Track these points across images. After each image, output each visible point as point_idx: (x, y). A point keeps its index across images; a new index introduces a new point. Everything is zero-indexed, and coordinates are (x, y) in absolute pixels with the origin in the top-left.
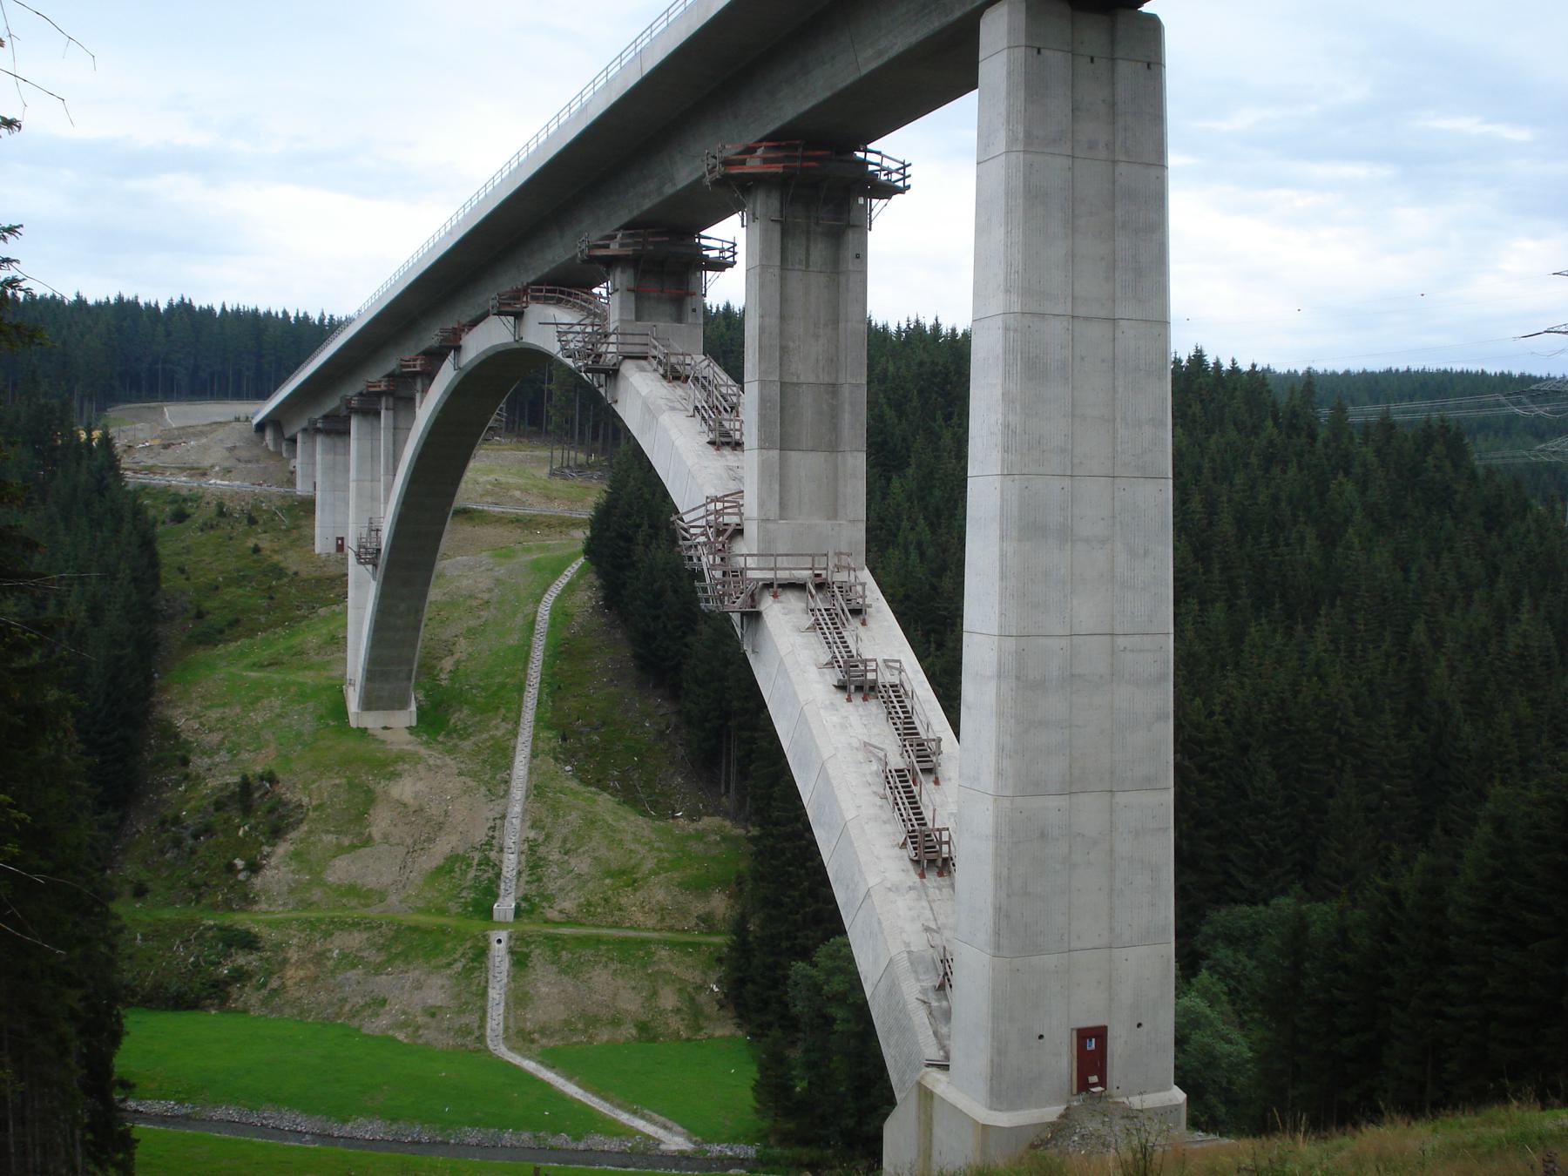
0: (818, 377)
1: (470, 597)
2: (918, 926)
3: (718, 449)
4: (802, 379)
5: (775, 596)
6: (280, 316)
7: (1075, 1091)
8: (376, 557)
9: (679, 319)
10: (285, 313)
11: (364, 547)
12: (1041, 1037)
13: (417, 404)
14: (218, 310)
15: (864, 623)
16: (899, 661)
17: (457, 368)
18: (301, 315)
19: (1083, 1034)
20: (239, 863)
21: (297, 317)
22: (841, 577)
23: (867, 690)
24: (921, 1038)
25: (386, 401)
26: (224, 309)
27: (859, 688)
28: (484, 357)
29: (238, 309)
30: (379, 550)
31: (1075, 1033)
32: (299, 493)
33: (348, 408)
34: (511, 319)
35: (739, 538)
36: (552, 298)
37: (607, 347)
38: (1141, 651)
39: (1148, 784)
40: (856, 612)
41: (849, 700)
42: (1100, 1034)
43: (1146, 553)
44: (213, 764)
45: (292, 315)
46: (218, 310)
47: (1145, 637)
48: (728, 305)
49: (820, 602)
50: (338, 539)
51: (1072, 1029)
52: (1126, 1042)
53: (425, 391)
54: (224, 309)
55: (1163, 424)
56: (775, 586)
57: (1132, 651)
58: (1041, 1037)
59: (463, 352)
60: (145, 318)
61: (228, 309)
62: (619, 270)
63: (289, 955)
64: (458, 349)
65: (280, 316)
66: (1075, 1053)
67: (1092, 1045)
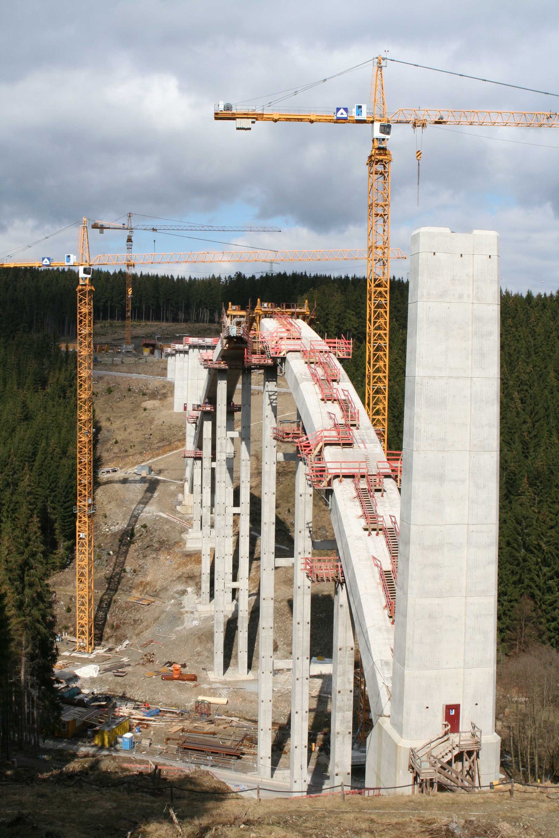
1: (83, 648)
6: (170, 277)
10: (172, 276)
12: (427, 708)
14: (139, 275)
16: (335, 415)
19: (449, 708)
26: (190, 278)
29: (148, 275)
32: (168, 380)
37: (424, 761)
42: (457, 707)
44: (17, 551)
45: (175, 278)
46: (139, 275)
48: (213, 275)
54: (141, 274)
56: (341, 476)
58: (427, 708)
61: (143, 274)
65: (170, 277)
67: (453, 713)
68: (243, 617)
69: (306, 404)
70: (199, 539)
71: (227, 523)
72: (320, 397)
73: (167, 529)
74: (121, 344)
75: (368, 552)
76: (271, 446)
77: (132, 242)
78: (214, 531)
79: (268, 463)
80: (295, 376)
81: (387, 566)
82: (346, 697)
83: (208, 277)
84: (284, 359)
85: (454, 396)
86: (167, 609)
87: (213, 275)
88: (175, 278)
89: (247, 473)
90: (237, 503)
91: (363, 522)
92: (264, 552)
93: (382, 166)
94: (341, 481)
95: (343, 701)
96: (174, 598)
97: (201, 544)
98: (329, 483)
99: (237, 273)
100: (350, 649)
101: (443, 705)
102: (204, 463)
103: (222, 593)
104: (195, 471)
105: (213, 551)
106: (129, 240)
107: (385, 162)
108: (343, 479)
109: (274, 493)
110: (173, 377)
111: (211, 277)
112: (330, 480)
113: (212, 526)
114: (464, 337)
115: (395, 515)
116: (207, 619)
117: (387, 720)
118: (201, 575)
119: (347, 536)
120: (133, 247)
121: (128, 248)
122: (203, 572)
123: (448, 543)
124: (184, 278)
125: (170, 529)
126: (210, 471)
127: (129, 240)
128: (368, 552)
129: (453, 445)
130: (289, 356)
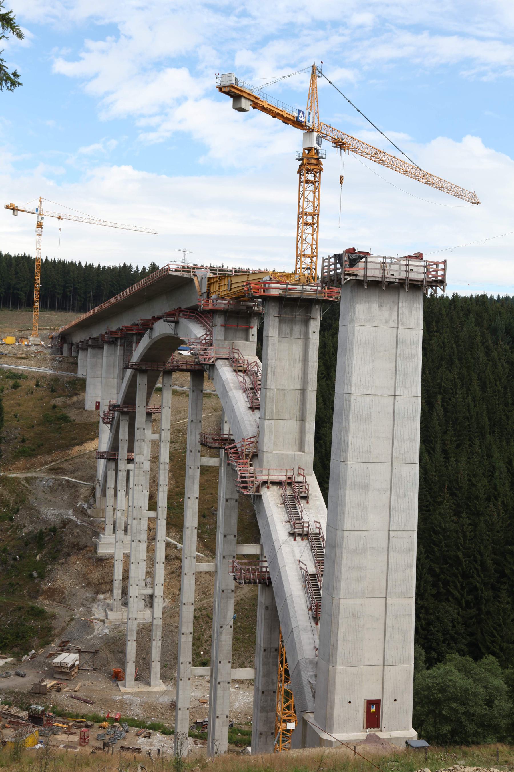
0: (294, 386)
2: (312, 647)
3: (253, 411)
4: (287, 388)
5: (268, 488)
6: (77, 265)
7: (365, 727)
8: (112, 421)
9: (247, 340)
10: (80, 263)
11: (106, 416)
12: (350, 702)
13: (134, 349)
15: (308, 502)
17: (150, 338)
18: (88, 264)
19: (370, 703)
20: (35, 574)
21: (86, 266)
22: (300, 479)
23: (305, 536)
24: (307, 698)
25: (121, 341)
27: (300, 535)
28: (162, 336)
29: (54, 261)
30: (114, 418)
31: (366, 701)
32: (79, 376)
33: (102, 341)
34: (173, 324)
35: (256, 458)
36: (193, 316)
38: (401, 538)
39: (404, 595)
40: (305, 498)
41: (295, 540)
42: (377, 703)
43: (405, 496)
45: (83, 265)
47: (403, 532)
48: (124, 264)
49: (289, 491)
50: (96, 402)
51: (364, 700)
52: (389, 707)
53: (138, 342)
55: (414, 440)
57: (397, 538)
58: (350, 702)
59: (154, 331)
60: (4, 264)
62: (217, 316)
63: (448, 657)
64: (152, 329)
65: (77, 265)
66: (366, 710)
68: (157, 625)
69: (235, 411)
70: (111, 543)
71: (142, 528)
72: (249, 406)
73: (77, 533)
74: (27, 335)
75: (294, 556)
76: (195, 450)
77: (42, 228)
78: (128, 537)
79: (192, 467)
80: (224, 384)
81: (312, 569)
82: (269, 698)
83: (118, 266)
84: (212, 366)
85: (379, 412)
86: (77, 617)
87: (124, 264)
88: (83, 265)
89: (165, 477)
90: (153, 506)
91: (288, 528)
92: (185, 557)
93: (313, 175)
94: (268, 488)
95: (266, 701)
96: (83, 605)
97: (114, 549)
98: (258, 490)
99: (151, 264)
100: (274, 650)
101: (364, 700)
102: (119, 465)
103: (136, 599)
104: (109, 473)
105: (127, 556)
106: (39, 225)
107: (315, 172)
108: (270, 485)
109: (197, 498)
110: (85, 374)
111: (122, 265)
112: (258, 486)
113: (126, 531)
114: (389, 358)
115: (320, 521)
116: (115, 628)
117: (312, 715)
118: (112, 581)
119: (274, 540)
120: (42, 234)
121: (37, 235)
122: (115, 577)
123: (370, 548)
124: (93, 266)
125: (80, 533)
126: (125, 473)
127: (39, 225)
128: (294, 556)
129: (377, 457)
130: (219, 364)
